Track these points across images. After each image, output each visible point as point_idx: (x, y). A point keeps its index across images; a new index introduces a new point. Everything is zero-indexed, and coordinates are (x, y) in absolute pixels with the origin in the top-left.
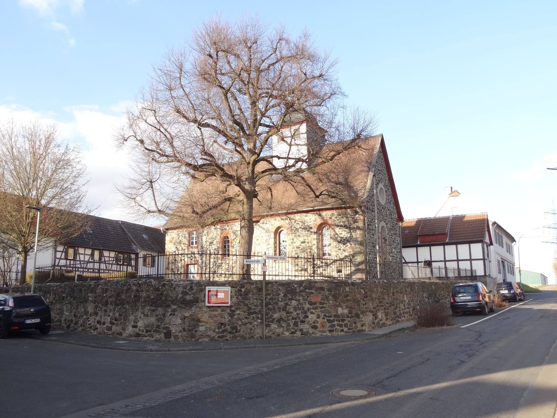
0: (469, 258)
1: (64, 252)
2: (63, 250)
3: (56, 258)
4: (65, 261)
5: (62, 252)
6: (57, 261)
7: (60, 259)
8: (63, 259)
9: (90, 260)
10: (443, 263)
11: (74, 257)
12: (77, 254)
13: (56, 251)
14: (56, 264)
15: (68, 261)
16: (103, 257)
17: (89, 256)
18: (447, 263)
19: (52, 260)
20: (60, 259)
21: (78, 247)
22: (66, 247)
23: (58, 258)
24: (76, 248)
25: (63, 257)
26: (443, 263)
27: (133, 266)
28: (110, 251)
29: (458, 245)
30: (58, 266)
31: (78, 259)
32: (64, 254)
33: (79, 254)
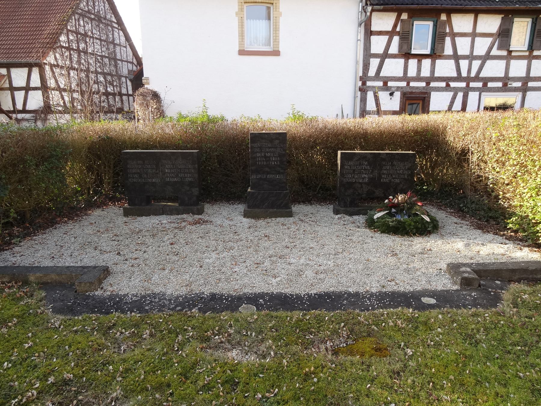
0: (31, 86)
1: (398, 33)
2: (395, 26)
3: (368, 55)
4: (402, 61)
5: (391, 34)
6: (374, 63)
7: (385, 56)
8: (394, 56)
9: (495, 52)
10: (477, 39)
11: (433, 49)
12: (444, 35)
13: (369, 33)
14: (473, 74)
15: (413, 63)
16: (448, 40)
17: (489, 40)
18: (469, 39)
19: (357, 62)
20: (385, 56)
21: (449, 12)
22: (404, 16)
23: (376, 56)
24: (443, 17)
25: (394, 49)
26: (477, 39)
27: (468, 85)
28: (476, 12)
29: (11, 69)
30: (477, 78)
31: (448, 50)
32: (396, 39)
33: (454, 35)
